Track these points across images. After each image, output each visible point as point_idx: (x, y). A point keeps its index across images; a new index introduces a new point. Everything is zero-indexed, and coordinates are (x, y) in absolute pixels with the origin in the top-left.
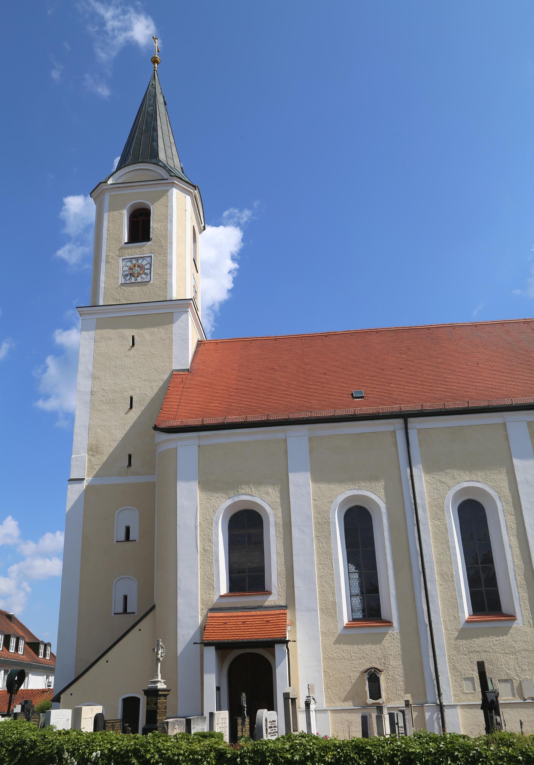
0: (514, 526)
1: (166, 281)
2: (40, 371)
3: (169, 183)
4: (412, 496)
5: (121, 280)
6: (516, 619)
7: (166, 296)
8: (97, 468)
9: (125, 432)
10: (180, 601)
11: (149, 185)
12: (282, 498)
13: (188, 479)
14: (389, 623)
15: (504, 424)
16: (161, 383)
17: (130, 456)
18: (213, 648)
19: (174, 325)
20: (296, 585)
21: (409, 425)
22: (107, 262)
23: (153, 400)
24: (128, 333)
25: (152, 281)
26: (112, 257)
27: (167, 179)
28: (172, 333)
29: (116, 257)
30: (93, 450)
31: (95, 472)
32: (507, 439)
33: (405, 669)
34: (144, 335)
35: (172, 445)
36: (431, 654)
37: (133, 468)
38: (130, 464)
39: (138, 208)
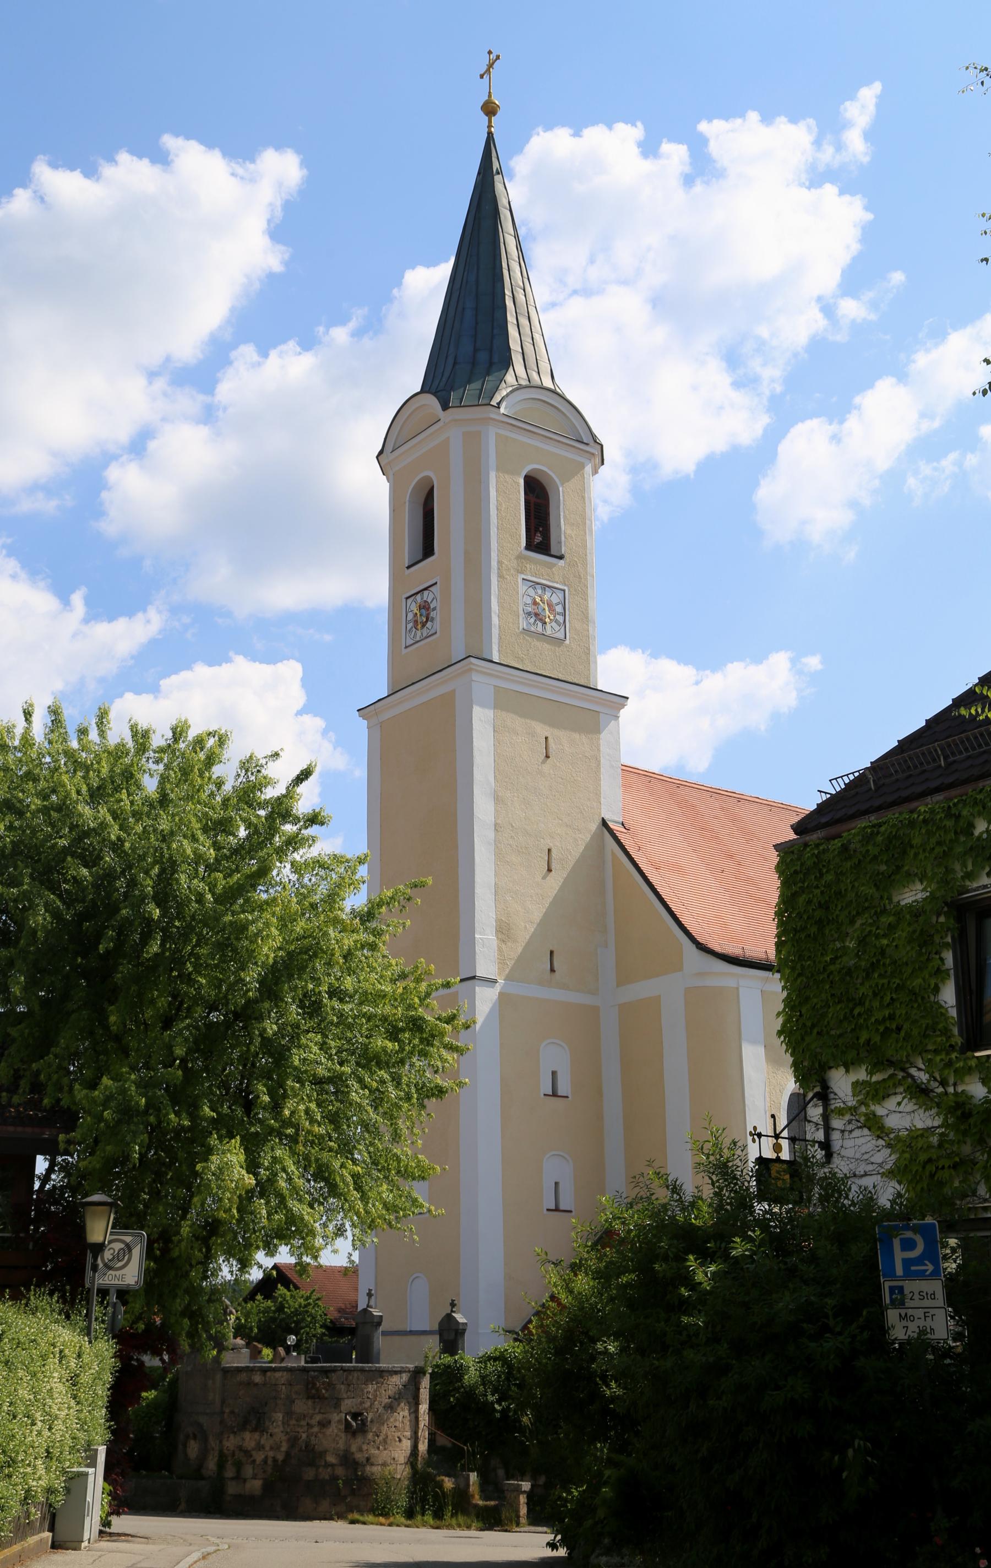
1: (589, 649)
2: (956, 935)
3: (587, 452)
5: (523, 624)
7: (588, 678)
8: (510, 964)
11: (559, 441)
13: (754, 1042)
16: (587, 837)
17: (552, 953)
22: (500, 576)
24: (542, 730)
25: (567, 642)
26: (508, 570)
27: (587, 444)
28: (599, 750)
29: (512, 571)
30: (504, 931)
31: (507, 971)
34: (562, 740)
35: (731, 983)
38: (552, 970)
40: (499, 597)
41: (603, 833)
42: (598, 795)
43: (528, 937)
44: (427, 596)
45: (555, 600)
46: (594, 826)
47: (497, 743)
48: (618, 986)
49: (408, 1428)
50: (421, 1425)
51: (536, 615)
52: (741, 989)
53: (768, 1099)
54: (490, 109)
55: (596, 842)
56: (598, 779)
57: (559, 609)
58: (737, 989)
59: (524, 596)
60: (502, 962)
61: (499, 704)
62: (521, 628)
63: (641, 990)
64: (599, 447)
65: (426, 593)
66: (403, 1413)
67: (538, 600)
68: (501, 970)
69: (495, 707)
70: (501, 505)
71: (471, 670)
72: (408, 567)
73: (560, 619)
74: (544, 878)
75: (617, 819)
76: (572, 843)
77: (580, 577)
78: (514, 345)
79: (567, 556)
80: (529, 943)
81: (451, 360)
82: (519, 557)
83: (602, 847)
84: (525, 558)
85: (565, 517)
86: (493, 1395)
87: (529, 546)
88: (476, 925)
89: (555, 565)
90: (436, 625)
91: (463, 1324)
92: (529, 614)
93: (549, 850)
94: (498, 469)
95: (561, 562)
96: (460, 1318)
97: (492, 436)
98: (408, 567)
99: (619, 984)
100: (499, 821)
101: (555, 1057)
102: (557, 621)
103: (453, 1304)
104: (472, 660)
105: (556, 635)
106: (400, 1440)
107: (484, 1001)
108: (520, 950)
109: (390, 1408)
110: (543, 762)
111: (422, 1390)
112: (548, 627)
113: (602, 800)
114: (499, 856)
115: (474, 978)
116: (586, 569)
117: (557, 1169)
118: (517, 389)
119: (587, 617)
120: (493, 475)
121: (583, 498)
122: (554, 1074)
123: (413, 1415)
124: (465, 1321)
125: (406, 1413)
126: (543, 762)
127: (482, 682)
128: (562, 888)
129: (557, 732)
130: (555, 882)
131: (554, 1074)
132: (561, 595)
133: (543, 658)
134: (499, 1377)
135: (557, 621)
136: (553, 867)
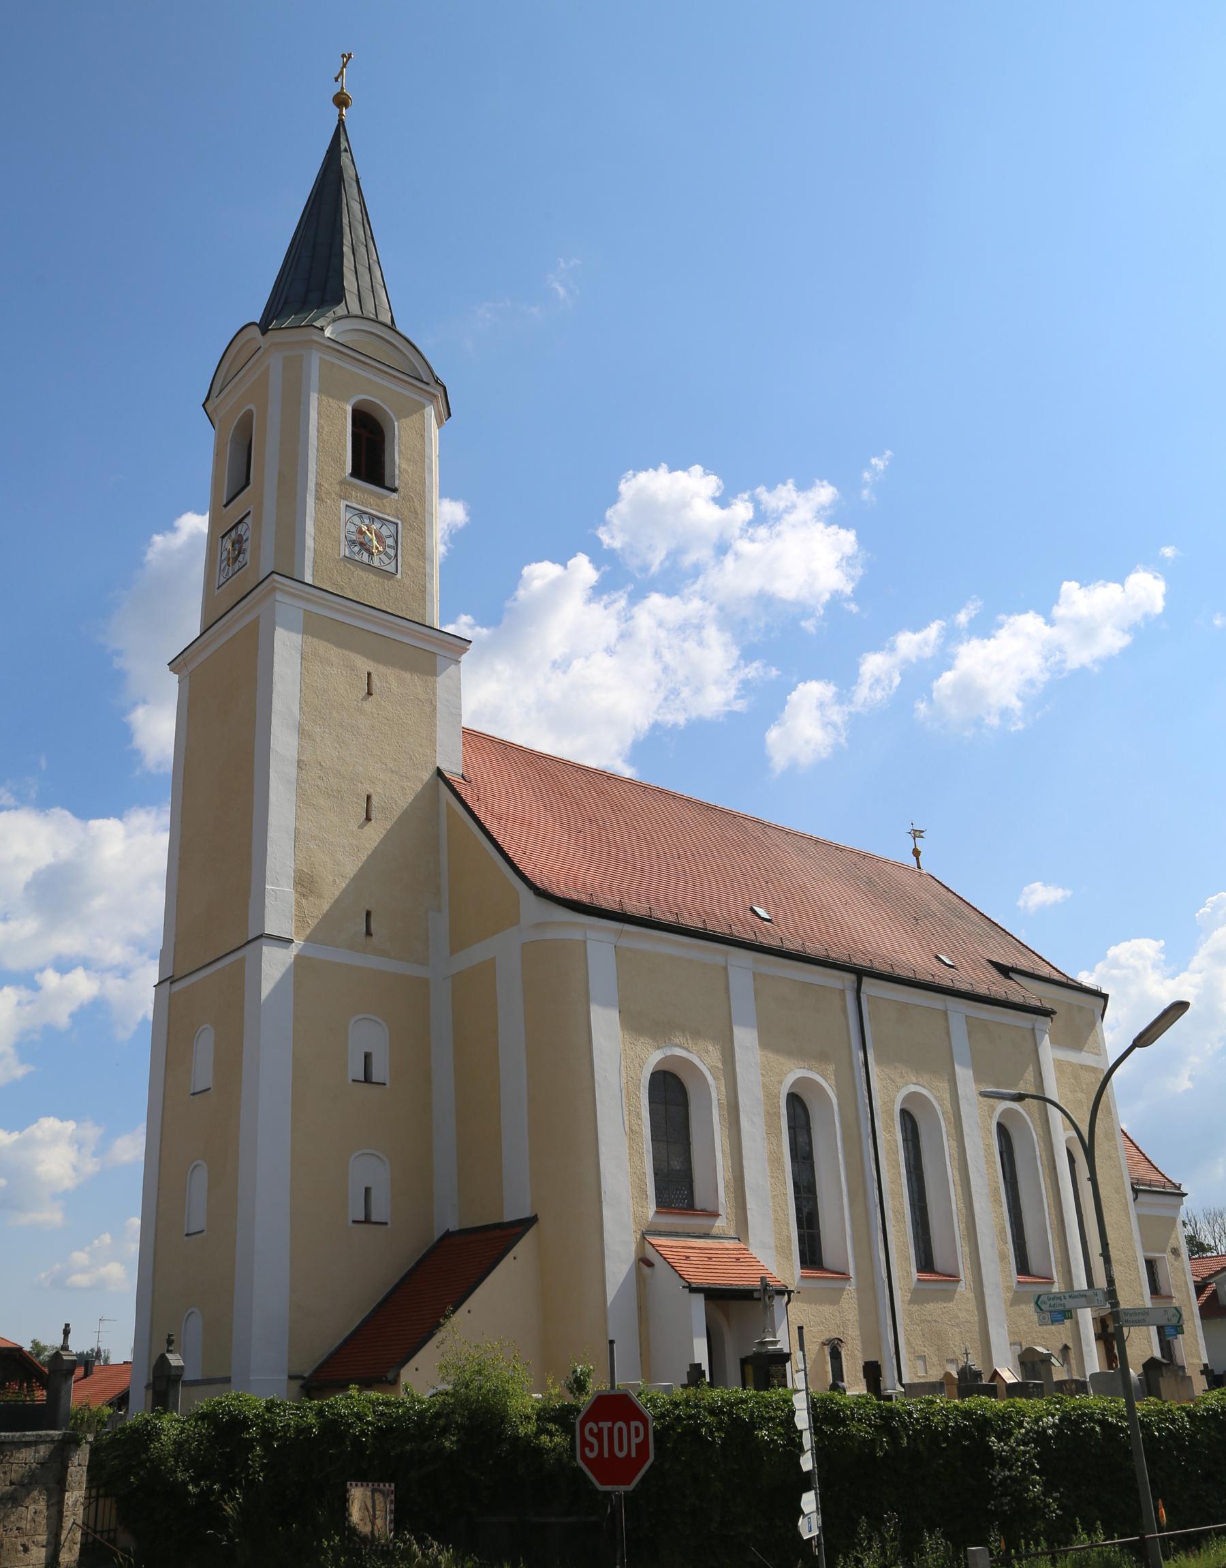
0: (956, 1156)
1: (425, 587)
4: (866, 1094)
5: (344, 550)
6: (958, 1281)
7: (424, 616)
8: (313, 923)
9: (360, 864)
10: (607, 1213)
12: (724, 1062)
13: (606, 1004)
14: (843, 1275)
15: (945, 1013)
16: (419, 787)
17: (368, 914)
18: (701, 1297)
19: (439, 679)
20: (748, 1206)
21: (863, 987)
22: (318, 498)
23: (405, 812)
24: (364, 664)
25: (399, 576)
28: (434, 694)
29: (333, 496)
30: (305, 883)
31: (308, 931)
32: (948, 1034)
33: (863, 1342)
34: (389, 678)
35: (576, 935)
36: (890, 1322)
37: (375, 939)
38: (368, 933)
39: (373, 414)
40: (316, 520)
41: (438, 784)
42: (432, 740)
43: (337, 893)
44: (241, 529)
45: (385, 531)
46: (427, 775)
47: (305, 673)
48: (452, 953)
49: (42, 1528)
50: (68, 1523)
51: (362, 544)
52: (590, 945)
53: (624, 1075)
54: (341, 101)
55: (430, 788)
56: (432, 725)
57: (390, 541)
58: (585, 942)
59: (347, 523)
60: (301, 919)
61: (312, 627)
62: (342, 554)
63: (476, 954)
64: (441, 389)
65: (240, 526)
66: (36, 1507)
67: (364, 528)
68: (299, 929)
69: (303, 633)
70: (323, 427)
71: (274, 589)
72: (225, 506)
73: (392, 552)
74: (361, 827)
75: (455, 770)
76: (399, 792)
77: (416, 513)
78: (349, 282)
79: (401, 489)
80: (337, 901)
81: (282, 301)
82: (342, 483)
83: (435, 800)
84: (350, 484)
85: (400, 451)
86: (187, 1470)
87: (356, 473)
88: (268, 873)
89: (387, 497)
90: (247, 557)
91: (177, 1367)
92: (353, 542)
93: (369, 798)
94: (320, 392)
95: (394, 496)
96: (175, 1360)
97: (315, 362)
98: (225, 506)
99: (453, 952)
100: (303, 758)
101: (368, 1036)
102: (386, 554)
103: (170, 1342)
104: (274, 576)
105: (387, 568)
106: (26, 1550)
107: (274, 965)
108: (326, 907)
109: (14, 1499)
110: (364, 699)
111: (71, 1469)
112: (376, 558)
113: (438, 748)
114: (302, 798)
115: (261, 936)
116: (423, 506)
117: (370, 1172)
118: (346, 317)
119: (424, 555)
120: (314, 398)
121: (423, 437)
122: (367, 1057)
123: (54, 1509)
124: (182, 1363)
125: (42, 1506)
126: (364, 699)
127: (286, 605)
128: (383, 841)
129: (381, 668)
130: (374, 834)
131: (367, 1057)
132: (393, 528)
133: (370, 589)
134: (201, 1443)
135: (386, 554)
136: (373, 815)
